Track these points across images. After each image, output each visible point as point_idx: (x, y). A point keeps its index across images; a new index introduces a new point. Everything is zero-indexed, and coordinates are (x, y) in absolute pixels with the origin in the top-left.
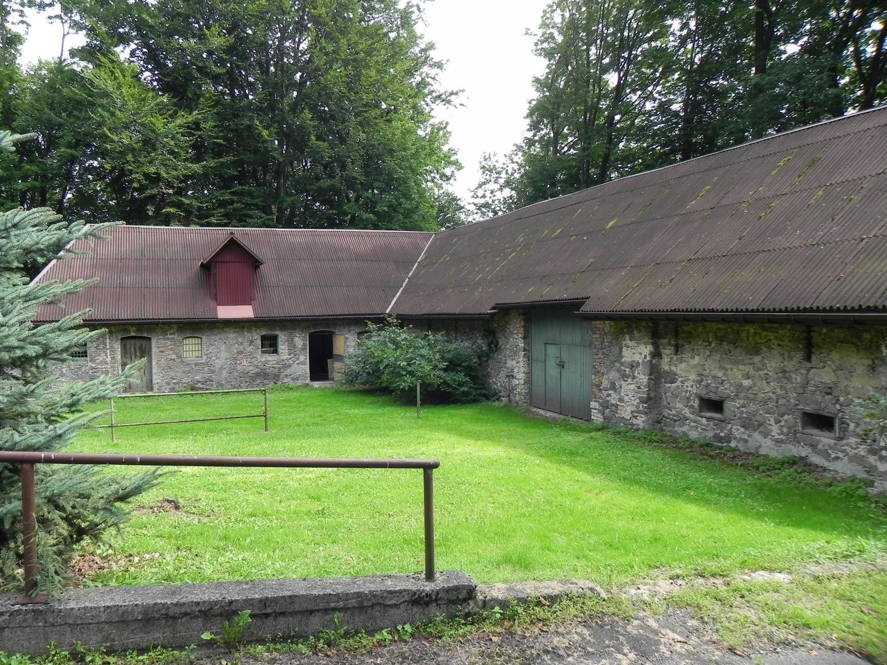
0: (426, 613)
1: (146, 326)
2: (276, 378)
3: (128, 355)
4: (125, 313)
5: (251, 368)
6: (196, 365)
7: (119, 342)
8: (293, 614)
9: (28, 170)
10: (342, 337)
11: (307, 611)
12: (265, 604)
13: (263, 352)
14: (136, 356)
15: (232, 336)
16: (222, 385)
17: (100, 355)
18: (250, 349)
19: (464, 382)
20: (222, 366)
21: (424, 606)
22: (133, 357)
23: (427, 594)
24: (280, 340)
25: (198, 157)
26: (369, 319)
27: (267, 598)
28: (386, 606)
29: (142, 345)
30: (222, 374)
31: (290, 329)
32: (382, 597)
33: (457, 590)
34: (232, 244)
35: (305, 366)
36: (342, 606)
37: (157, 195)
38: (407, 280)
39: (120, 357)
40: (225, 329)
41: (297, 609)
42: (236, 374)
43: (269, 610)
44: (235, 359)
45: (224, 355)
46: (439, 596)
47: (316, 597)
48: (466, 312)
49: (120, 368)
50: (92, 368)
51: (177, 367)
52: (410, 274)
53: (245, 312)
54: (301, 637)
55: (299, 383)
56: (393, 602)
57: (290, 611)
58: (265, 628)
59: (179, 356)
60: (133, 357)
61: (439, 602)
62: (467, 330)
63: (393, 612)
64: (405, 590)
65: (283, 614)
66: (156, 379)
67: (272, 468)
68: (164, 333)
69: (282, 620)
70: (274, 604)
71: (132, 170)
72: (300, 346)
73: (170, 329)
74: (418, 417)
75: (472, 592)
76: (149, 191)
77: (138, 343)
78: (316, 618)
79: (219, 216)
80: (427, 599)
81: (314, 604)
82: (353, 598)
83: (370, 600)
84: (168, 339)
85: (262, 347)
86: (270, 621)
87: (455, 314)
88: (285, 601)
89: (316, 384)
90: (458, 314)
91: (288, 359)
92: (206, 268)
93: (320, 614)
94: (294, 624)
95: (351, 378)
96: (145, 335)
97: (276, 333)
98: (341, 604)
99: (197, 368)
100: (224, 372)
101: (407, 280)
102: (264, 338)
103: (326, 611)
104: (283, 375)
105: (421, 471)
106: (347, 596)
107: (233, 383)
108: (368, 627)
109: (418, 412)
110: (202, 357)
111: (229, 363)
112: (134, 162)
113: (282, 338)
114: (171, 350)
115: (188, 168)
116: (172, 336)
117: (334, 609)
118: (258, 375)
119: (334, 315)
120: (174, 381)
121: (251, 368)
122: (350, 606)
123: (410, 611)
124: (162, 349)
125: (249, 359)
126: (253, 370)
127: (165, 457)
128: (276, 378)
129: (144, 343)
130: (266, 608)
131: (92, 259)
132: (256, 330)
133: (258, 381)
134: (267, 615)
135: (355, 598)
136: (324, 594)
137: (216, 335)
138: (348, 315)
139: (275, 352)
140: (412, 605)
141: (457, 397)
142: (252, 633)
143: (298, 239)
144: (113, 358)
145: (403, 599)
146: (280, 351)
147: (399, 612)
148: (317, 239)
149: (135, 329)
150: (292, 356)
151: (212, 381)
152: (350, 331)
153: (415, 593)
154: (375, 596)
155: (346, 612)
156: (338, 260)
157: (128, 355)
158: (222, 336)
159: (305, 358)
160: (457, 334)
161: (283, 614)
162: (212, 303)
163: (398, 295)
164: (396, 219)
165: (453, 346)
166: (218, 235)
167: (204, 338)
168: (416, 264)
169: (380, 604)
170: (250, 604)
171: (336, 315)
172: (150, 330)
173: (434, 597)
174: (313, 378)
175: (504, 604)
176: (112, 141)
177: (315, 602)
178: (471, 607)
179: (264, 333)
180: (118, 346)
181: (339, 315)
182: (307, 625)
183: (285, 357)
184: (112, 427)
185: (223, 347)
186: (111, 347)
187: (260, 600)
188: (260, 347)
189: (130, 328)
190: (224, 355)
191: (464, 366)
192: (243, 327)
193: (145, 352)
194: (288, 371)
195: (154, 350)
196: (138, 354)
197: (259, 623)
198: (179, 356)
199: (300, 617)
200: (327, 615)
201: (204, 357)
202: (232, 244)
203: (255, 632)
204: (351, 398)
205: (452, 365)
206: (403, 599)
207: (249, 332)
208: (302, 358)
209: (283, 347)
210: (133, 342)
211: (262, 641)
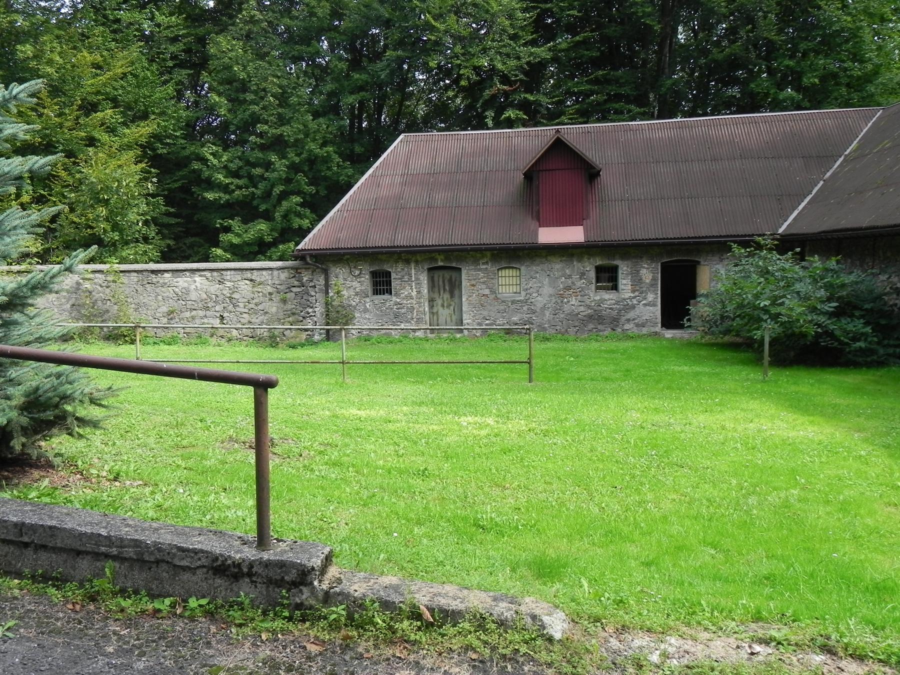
0: (235, 589)
1: (455, 254)
2: (614, 322)
3: (436, 289)
4: (431, 238)
5: (582, 308)
6: (513, 302)
7: (426, 273)
8: (55, 550)
9: (357, 80)
10: (707, 268)
11: (72, 550)
12: (21, 530)
13: (598, 288)
14: (445, 290)
15: (557, 266)
16: (545, 329)
17: (404, 288)
18: (580, 283)
19: (862, 334)
20: (545, 305)
21: (232, 580)
22: (442, 292)
23: (234, 562)
24: (620, 272)
25: (512, 37)
26: (735, 242)
27: (23, 524)
28: (175, 566)
29: (451, 277)
30: (544, 315)
31: (636, 257)
32: (169, 553)
33: (281, 567)
34: (559, 146)
35: (655, 308)
36: (116, 553)
37: (497, 94)
38: (822, 183)
39: (426, 291)
40: (549, 258)
41: (59, 545)
42: (562, 316)
43: (26, 539)
44: (562, 296)
45: (547, 290)
46: (254, 570)
47: (82, 535)
48: (879, 224)
49: (427, 304)
50: (397, 304)
51: (491, 305)
52: (828, 174)
53: (574, 234)
54: (60, 582)
55: (645, 331)
56: (184, 563)
57: (51, 545)
58: (24, 561)
59: (493, 292)
60: (442, 292)
61: (254, 579)
62: (889, 254)
63: (186, 576)
64: (202, 551)
65: (44, 547)
66: (466, 318)
67: (238, 386)
68: (476, 261)
69: (43, 556)
70: (31, 532)
71: (460, 65)
72: (648, 281)
73: (483, 257)
74: (764, 381)
75: (306, 575)
76: (487, 92)
77: (447, 274)
78: (85, 562)
79: (571, 114)
80: (236, 570)
81: (79, 543)
82: (129, 547)
83: (152, 553)
84: (480, 270)
85: (597, 281)
86: (29, 552)
87: (861, 229)
88: (45, 531)
89: (669, 334)
90: (866, 228)
91: (631, 298)
92: (529, 176)
93: (89, 557)
94: (58, 564)
95: (711, 325)
96: (454, 265)
97: (616, 262)
98: (114, 551)
99: (514, 306)
100: (547, 313)
101: (822, 183)
102: (599, 270)
103: (97, 556)
104: (624, 319)
105: (251, 388)
106: (121, 543)
107: (558, 328)
108: (152, 589)
109: (765, 374)
110: (520, 293)
111: (554, 301)
112: (463, 55)
113: (624, 268)
114: (484, 283)
115: (532, 54)
116: (484, 267)
117: (107, 556)
118: (590, 317)
119: (696, 238)
120: (487, 322)
121: (582, 308)
122: (125, 555)
123: (210, 582)
124: (473, 282)
125: (579, 297)
126: (584, 311)
127: (64, 356)
128: (614, 322)
129: (454, 274)
130: (22, 536)
131: (403, 175)
132: (589, 259)
133: (591, 326)
134: (26, 545)
135: (133, 547)
136: (92, 533)
137: (538, 265)
138: (717, 237)
139: (615, 288)
140: (215, 574)
141: (850, 356)
142: (10, 564)
143: (659, 134)
144: (419, 292)
145: (199, 562)
146: (621, 287)
147: (194, 578)
148: (713, 132)
149: (442, 257)
150: (637, 294)
151: (532, 324)
152: (721, 260)
153: (217, 559)
154: (160, 550)
155: (122, 563)
156: (714, 159)
157: (436, 289)
158: (546, 266)
159: (655, 297)
160: (873, 262)
161: (44, 547)
162: (533, 224)
163: (801, 207)
164: (836, 94)
165: (848, 279)
166: (541, 136)
167: (523, 268)
168: (843, 157)
169: (168, 562)
170: (3, 526)
171: (699, 238)
172: (460, 259)
173: (245, 570)
174: (663, 325)
175: (356, 605)
176: (438, 30)
177: (81, 540)
178: (304, 597)
179: (599, 262)
180: (424, 278)
181: (703, 237)
182: (74, 569)
183: (627, 295)
184: (343, 363)
185: (546, 281)
186: (417, 279)
187: (16, 525)
188: (594, 281)
189: (438, 256)
190: (547, 290)
191: (866, 310)
192: (572, 255)
193: (454, 287)
194: (631, 315)
195: (465, 283)
196: (447, 288)
197: (17, 552)
198: (493, 292)
199: (65, 555)
200: (99, 560)
201: (523, 293)
202: (559, 146)
203: (13, 562)
204: (703, 353)
205: (846, 309)
206: (199, 562)
207: (579, 261)
208: (650, 297)
209: (624, 282)
210: (441, 273)
211: (19, 575)
